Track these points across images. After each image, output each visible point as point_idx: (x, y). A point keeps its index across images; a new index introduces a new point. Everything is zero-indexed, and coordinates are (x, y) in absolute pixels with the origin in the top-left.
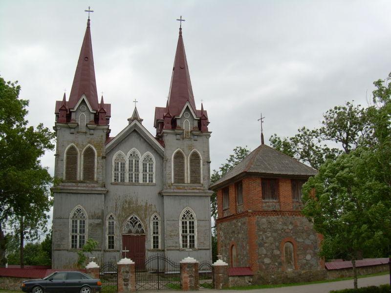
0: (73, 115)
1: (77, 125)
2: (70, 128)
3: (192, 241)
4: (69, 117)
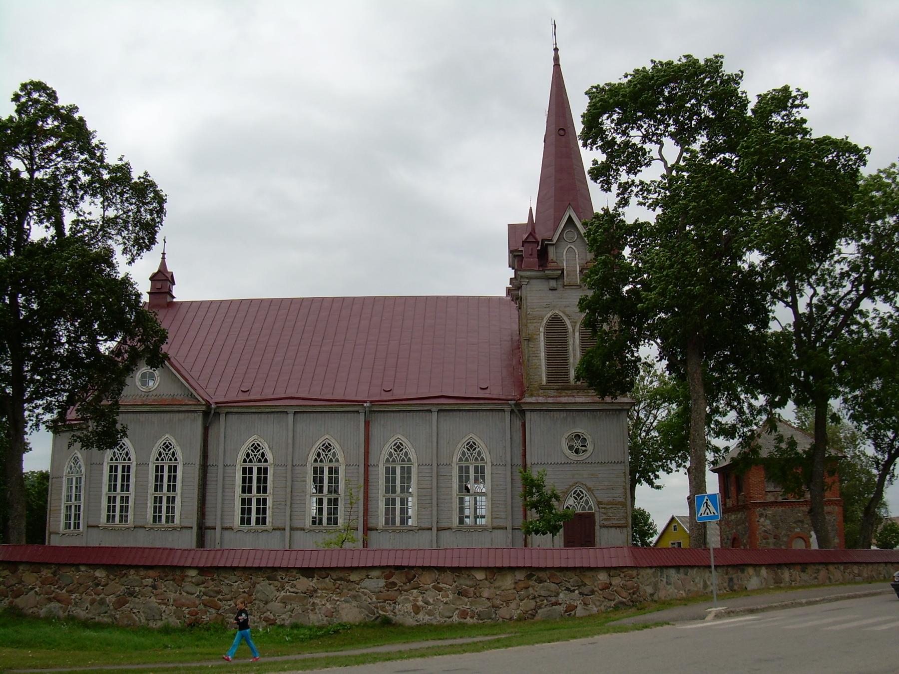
0: (551, 251)
1: (560, 272)
2: (548, 278)
3: (261, 511)
4: (543, 255)
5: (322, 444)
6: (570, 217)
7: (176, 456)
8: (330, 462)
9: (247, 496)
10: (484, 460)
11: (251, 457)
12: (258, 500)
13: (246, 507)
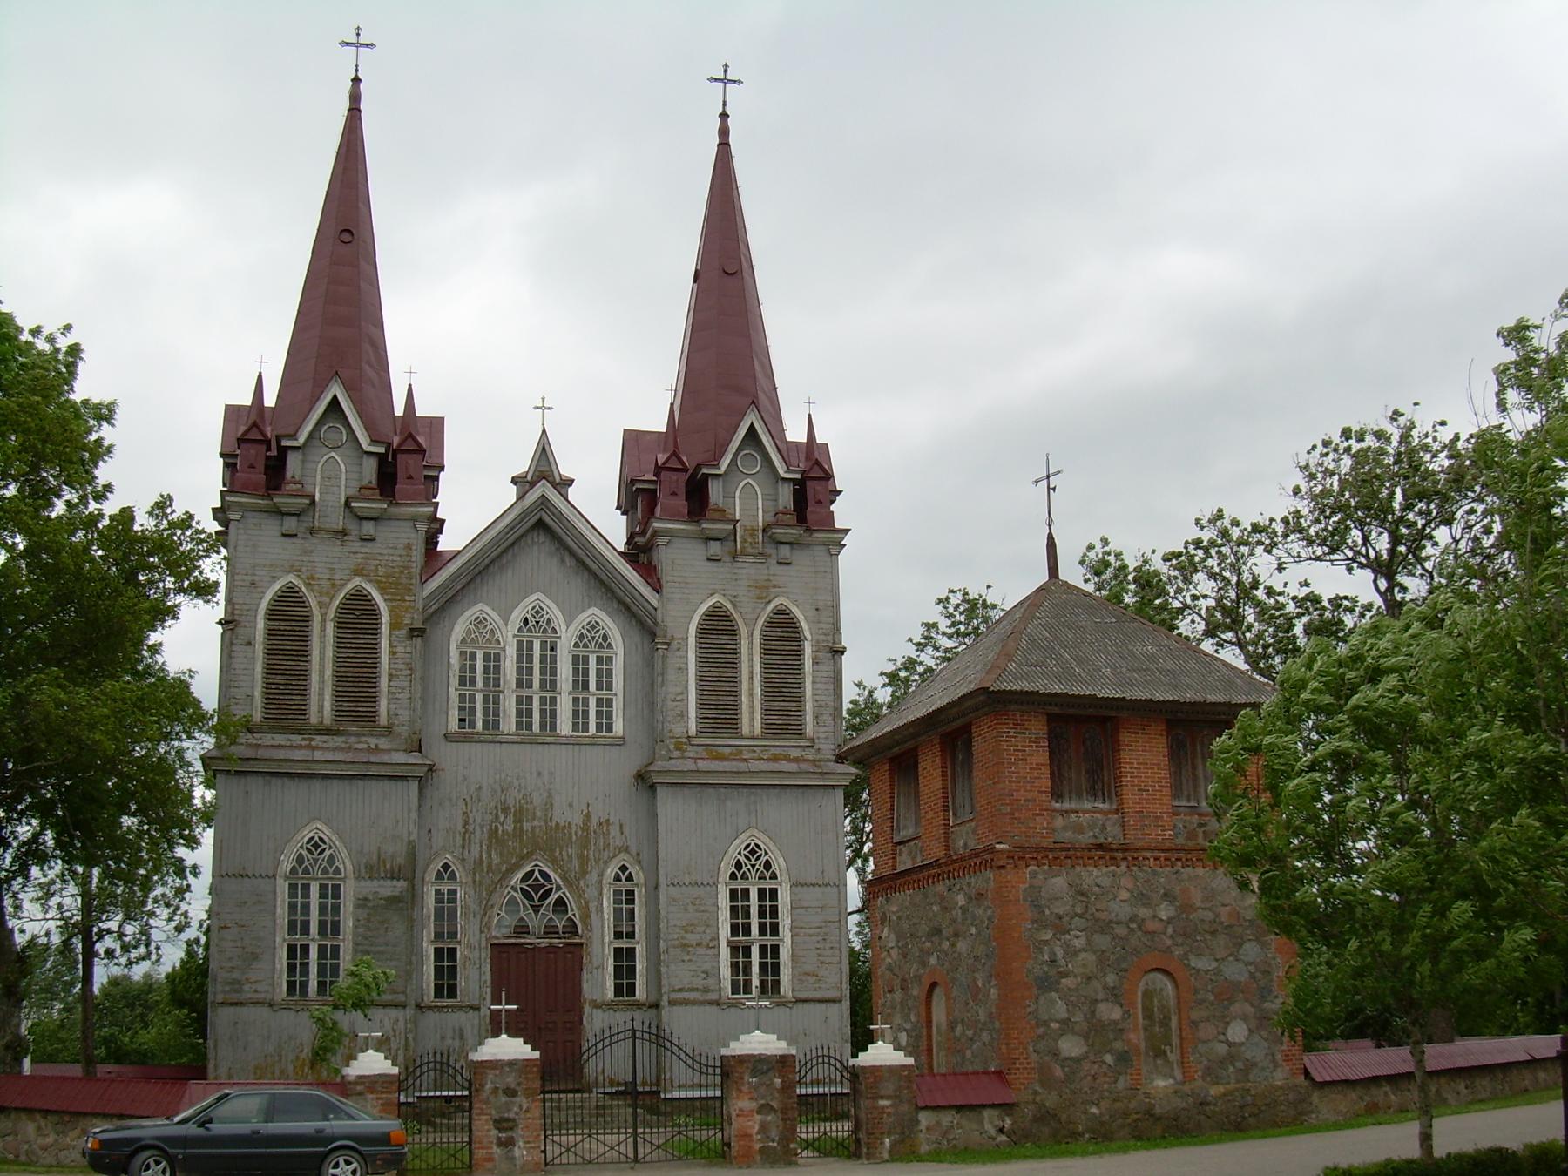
0: (293, 464)
2: (281, 513)
3: (771, 968)
4: (275, 470)
5: (743, 846)
6: (335, 397)
7: (773, 868)
8: (759, 878)
9: (769, 941)
10: (776, 878)
11: (744, 869)
12: (763, 949)
13: (329, 961)
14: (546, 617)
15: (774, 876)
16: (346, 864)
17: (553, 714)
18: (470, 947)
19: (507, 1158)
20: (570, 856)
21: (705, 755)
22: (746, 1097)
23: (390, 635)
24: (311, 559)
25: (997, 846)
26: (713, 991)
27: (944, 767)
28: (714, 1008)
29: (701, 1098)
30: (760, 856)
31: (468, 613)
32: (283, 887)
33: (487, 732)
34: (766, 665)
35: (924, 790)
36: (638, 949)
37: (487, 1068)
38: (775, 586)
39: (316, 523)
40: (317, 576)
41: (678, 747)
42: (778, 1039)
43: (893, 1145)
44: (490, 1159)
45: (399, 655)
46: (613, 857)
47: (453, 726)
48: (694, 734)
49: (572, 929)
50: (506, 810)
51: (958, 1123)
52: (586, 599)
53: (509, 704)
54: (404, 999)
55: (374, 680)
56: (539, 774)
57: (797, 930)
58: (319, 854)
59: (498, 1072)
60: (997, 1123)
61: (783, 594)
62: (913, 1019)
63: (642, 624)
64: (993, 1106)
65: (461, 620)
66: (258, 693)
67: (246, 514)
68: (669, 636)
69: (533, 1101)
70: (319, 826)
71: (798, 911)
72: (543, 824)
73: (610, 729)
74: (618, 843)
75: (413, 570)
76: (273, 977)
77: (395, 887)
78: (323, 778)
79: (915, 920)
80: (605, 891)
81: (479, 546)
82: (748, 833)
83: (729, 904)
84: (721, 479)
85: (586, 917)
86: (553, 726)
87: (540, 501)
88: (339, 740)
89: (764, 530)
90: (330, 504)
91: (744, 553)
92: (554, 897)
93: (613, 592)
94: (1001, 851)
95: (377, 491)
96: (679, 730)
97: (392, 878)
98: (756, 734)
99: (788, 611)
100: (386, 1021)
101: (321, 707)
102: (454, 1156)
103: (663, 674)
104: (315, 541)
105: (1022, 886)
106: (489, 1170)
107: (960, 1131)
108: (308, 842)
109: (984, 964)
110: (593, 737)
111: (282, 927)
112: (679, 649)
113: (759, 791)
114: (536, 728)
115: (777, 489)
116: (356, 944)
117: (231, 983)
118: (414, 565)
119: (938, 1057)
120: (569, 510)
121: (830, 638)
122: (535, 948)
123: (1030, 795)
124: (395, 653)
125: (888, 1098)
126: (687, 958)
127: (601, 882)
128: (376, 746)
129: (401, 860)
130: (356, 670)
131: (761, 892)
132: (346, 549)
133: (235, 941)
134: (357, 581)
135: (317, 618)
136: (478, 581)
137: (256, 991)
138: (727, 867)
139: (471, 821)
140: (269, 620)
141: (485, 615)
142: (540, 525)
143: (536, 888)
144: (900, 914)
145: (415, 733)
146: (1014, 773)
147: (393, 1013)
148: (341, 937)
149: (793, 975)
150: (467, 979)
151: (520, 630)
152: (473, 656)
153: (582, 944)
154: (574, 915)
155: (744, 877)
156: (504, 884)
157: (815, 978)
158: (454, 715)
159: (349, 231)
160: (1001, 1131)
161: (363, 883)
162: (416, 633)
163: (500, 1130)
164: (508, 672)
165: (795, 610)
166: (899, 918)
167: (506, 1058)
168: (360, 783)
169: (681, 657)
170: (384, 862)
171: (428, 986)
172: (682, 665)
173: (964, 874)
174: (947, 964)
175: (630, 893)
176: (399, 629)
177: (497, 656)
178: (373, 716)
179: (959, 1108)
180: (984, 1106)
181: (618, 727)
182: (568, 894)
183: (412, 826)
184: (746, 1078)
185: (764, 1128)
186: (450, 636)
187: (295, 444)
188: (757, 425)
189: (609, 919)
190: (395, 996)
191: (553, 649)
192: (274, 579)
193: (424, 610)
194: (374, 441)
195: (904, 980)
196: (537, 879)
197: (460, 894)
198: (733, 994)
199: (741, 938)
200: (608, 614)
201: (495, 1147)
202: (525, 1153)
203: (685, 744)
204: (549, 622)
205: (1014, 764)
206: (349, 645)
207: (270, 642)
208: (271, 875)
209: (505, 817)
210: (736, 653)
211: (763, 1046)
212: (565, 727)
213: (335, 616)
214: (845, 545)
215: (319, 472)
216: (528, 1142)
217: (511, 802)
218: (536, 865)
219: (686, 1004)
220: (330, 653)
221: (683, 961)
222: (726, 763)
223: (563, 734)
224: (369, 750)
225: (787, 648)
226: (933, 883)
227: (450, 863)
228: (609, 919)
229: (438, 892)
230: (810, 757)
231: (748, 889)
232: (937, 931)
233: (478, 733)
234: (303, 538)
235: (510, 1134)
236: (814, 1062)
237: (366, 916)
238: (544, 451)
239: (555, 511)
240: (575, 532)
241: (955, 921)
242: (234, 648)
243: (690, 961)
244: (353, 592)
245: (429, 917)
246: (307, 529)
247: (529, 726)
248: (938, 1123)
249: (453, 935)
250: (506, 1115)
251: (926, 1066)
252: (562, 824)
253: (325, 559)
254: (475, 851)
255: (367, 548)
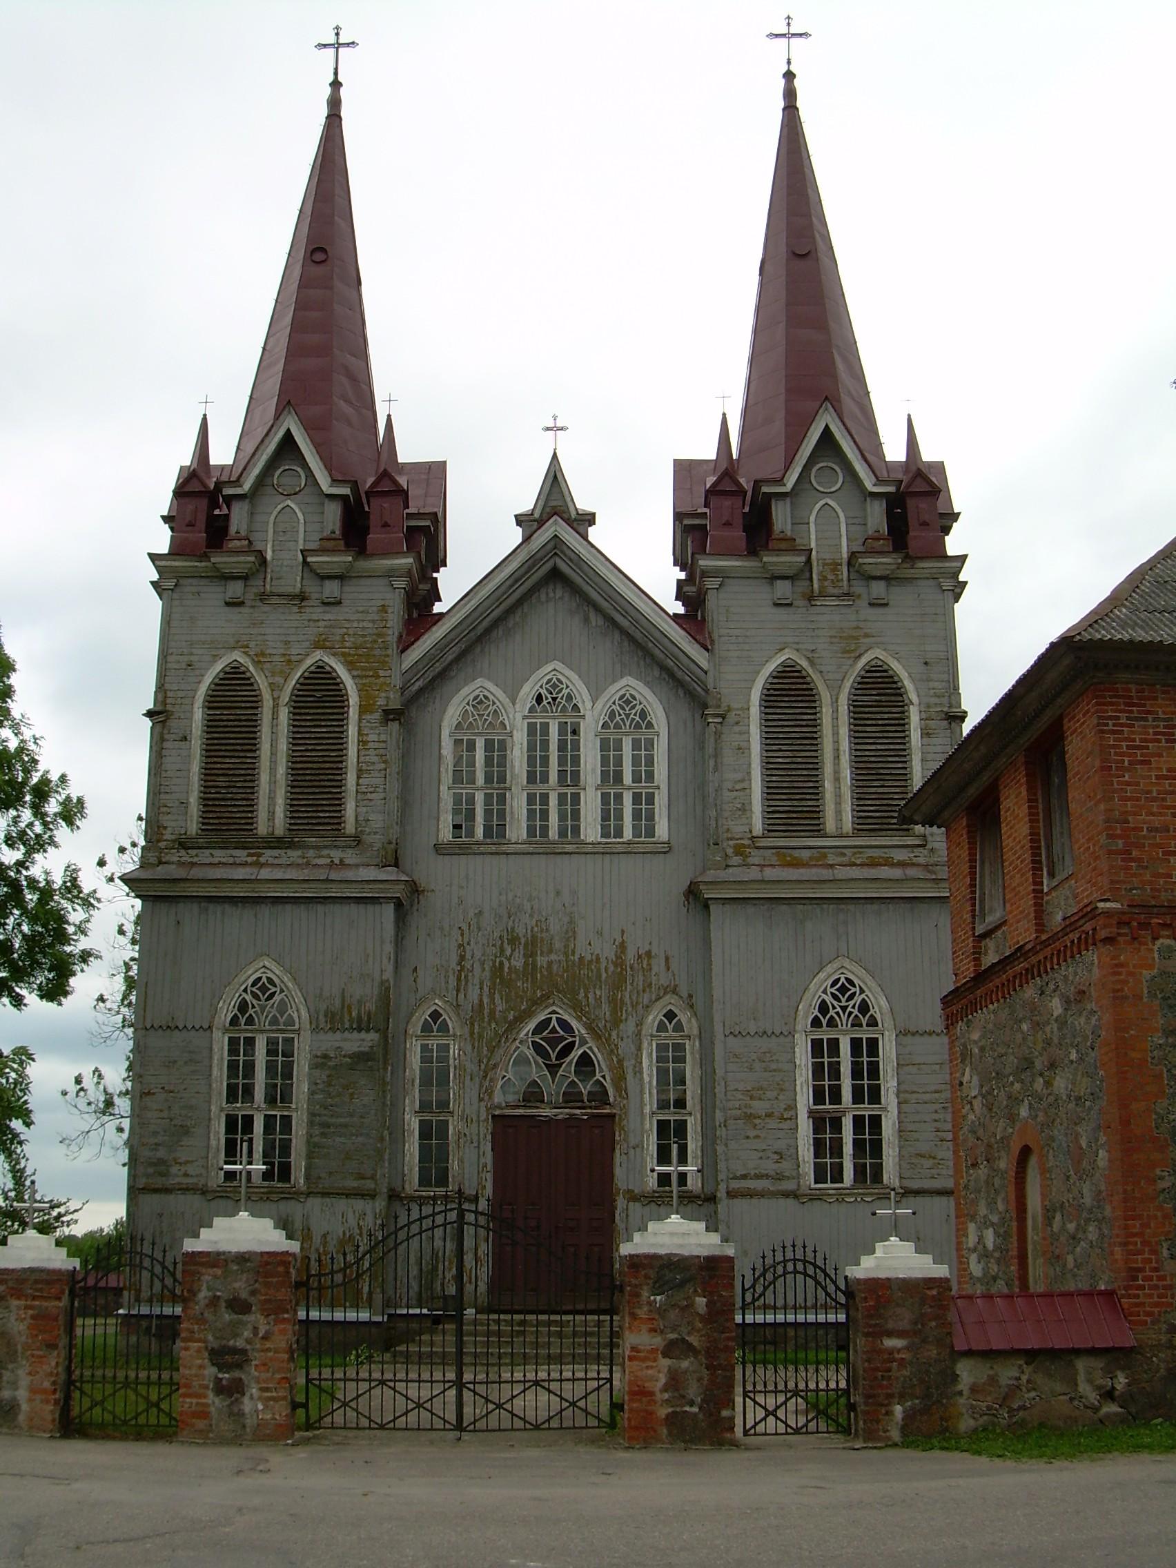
1: (803, 559)
3: (869, 1146)
5: (830, 982)
6: (827, 432)
7: (872, 1011)
8: (853, 1025)
9: (866, 1110)
10: (877, 1025)
11: (832, 1012)
12: (858, 1121)
13: (278, 1137)
14: (565, 692)
15: (873, 1023)
16: (300, 1013)
17: (576, 815)
18: (465, 1119)
19: (231, 1414)
20: (598, 1000)
21: (774, 861)
22: (644, 1328)
23: (360, 720)
24: (262, 631)
25: (1101, 905)
26: (788, 1178)
27: (1032, 801)
28: (790, 1201)
29: (796, 1325)
30: (854, 994)
31: (465, 691)
32: (221, 1042)
33: (489, 841)
34: (857, 739)
35: (1007, 842)
36: (691, 1122)
37: (203, 1264)
38: (866, 636)
39: (268, 587)
40: (268, 651)
41: (739, 851)
42: (707, 1229)
43: (909, 1417)
44: (203, 1414)
45: (371, 745)
46: (657, 1000)
47: (446, 834)
48: (760, 834)
49: (600, 1096)
50: (513, 941)
51: (1028, 1381)
52: (618, 667)
53: (518, 804)
54: (373, 1186)
55: (339, 778)
56: (558, 893)
57: (907, 1096)
58: (267, 1000)
59: (219, 1272)
60: (1100, 1382)
61: (878, 645)
62: (1001, 1206)
63: (690, 694)
64: (1093, 1352)
65: (456, 700)
66: (194, 799)
67: (181, 581)
68: (724, 705)
69: (276, 1322)
70: (267, 964)
71: (906, 1069)
72: (562, 958)
73: (651, 832)
74: (664, 981)
75: (389, 638)
76: (207, 1157)
77: (363, 1040)
78: (273, 903)
79: (1001, 1050)
80: (645, 1045)
81: (473, 603)
82: (836, 965)
83: (810, 1060)
84: (788, 500)
85: (619, 1081)
86: (576, 830)
87: (552, 543)
88: (294, 855)
89: (849, 564)
90: (285, 563)
91: (823, 594)
92: (576, 1053)
93: (652, 656)
94: (1108, 914)
95: (342, 542)
96: (741, 829)
97: (360, 1030)
98: (844, 831)
99: (885, 667)
100: (350, 1215)
101: (272, 814)
102: (157, 1405)
103: (716, 756)
104: (266, 608)
105: (1146, 974)
106: (201, 1431)
107: (1033, 1394)
108: (254, 984)
109: (1090, 1109)
110: (629, 843)
111: (220, 1093)
112: (737, 723)
113: (852, 907)
114: (553, 833)
115: (865, 510)
116: (312, 1114)
117: (155, 1164)
118: (390, 632)
119: (1035, 1269)
120: (590, 552)
121: (945, 700)
122: (550, 1121)
123: (1157, 821)
124: (365, 743)
125: (900, 1334)
126: (752, 1133)
127: (639, 1034)
128: (341, 860)
129: (371, 1006)
130: (315, 766)
131: (856, 1044)
132: (305, 616)
133: (161, 1111)
134: (318, 655)
135: (267, 703)
136: (478, 650)
137: (186, 1175)
138: (807, 1010)
139: (468, 956)
140: (209, 708)
141: (486, 693)
142: (555, 575)
143: (555, 1042)
144: (983, 1043)
145: (390, 843)
146: (1128, 784)
147: (359, 1204)
148: (293, 1106)
149: (901, 1156)
150: (461, 1161)
151: (532, 710)
152: (471, 746)
153: (612, 1116)
154: (604, 1077)
155: (832, 1023)
156: (511, 1037)
157: (931, 1161)
158: (447, 821)
159: (323, 250)
160: (1109, 1395)
161: (322, 1036)
162: (390, 715)
163: (222, 1367)
164: (517, 764)
165: (896, 666)
166: (982, 1049)
167: (234, 1248)
168: (320, 908)
169: (740, 733)
170: (349, 1007)
171: (411, 1170)
172: (743, 744)
173: (1059, 964)
174: (1041, 1114)
175: (679, 1048)
176: (371, 712)
177: (502, 744)
178: (337, 822)
179: (1031, 1355)
180: (1077, 1352)
181: (662, 830)
182: (596, 1050)
183: (385, 961)
184: (645, 1294)
185: (675, 1382)
186: (441, 721)
187: (238, 491)
188: (833, 428)
189: (650, 1082)
190: (363, 1181)
191: (575, 732)
192: (216, 658)
193: (403, 690)
194: (335, 481)
195: (989, 1146)
196: (554, 1030)
197: (454, 1050)
198: (816, 1182)
199: (827, 1106)
200: (647, 684)
201: (211, 1394)
202: (260, 1407)
203: (749, 846)
204: (569, 698)
205: (1128, 770)
206: (307, 735)
207: (209, 736)
208: (206, 1026)
209: (513, 951)
210: (815, 724)
211: (676, 1240)
212: (591, 831)
213: (290, 700)
214: (966, 583)
215: (271, 525)
216: (267, 1390)
217: (520, 931)
218: (554, 1012)
219: (751, 1197)
220: (283, 746)
221: (748, 1137)
222: (802, 871)
223: (589, 840)
224: (331, 865)
225: (886, 716)
226: (1021, 986)
227: (441, 1011)
228: (650, 1082)
229: (425, 1048)
230: (921, 860)
231: (837, 1040)
232: (1027, 1064)
233: (477, 843)
234: (253, 607)
235: (237, 1374)
236: (780, 1269)
237: (324, 1077)
238: (555, 480)
239: (573, 556)
240: (597, 579)
241: (1048, 1042)
242: (165, 745)
243: (757, 1137)
244: (312, 668)
245: (413, 1081)
246: (256, 594)
247: (545, 830)
248: (993, 1380)
249: (444, 1105)
250: (231, 1343)
251: (1017, 1283)
252: (588, 957)
253: (279, 631)
254: (473, 993)
255: (332, 614)
